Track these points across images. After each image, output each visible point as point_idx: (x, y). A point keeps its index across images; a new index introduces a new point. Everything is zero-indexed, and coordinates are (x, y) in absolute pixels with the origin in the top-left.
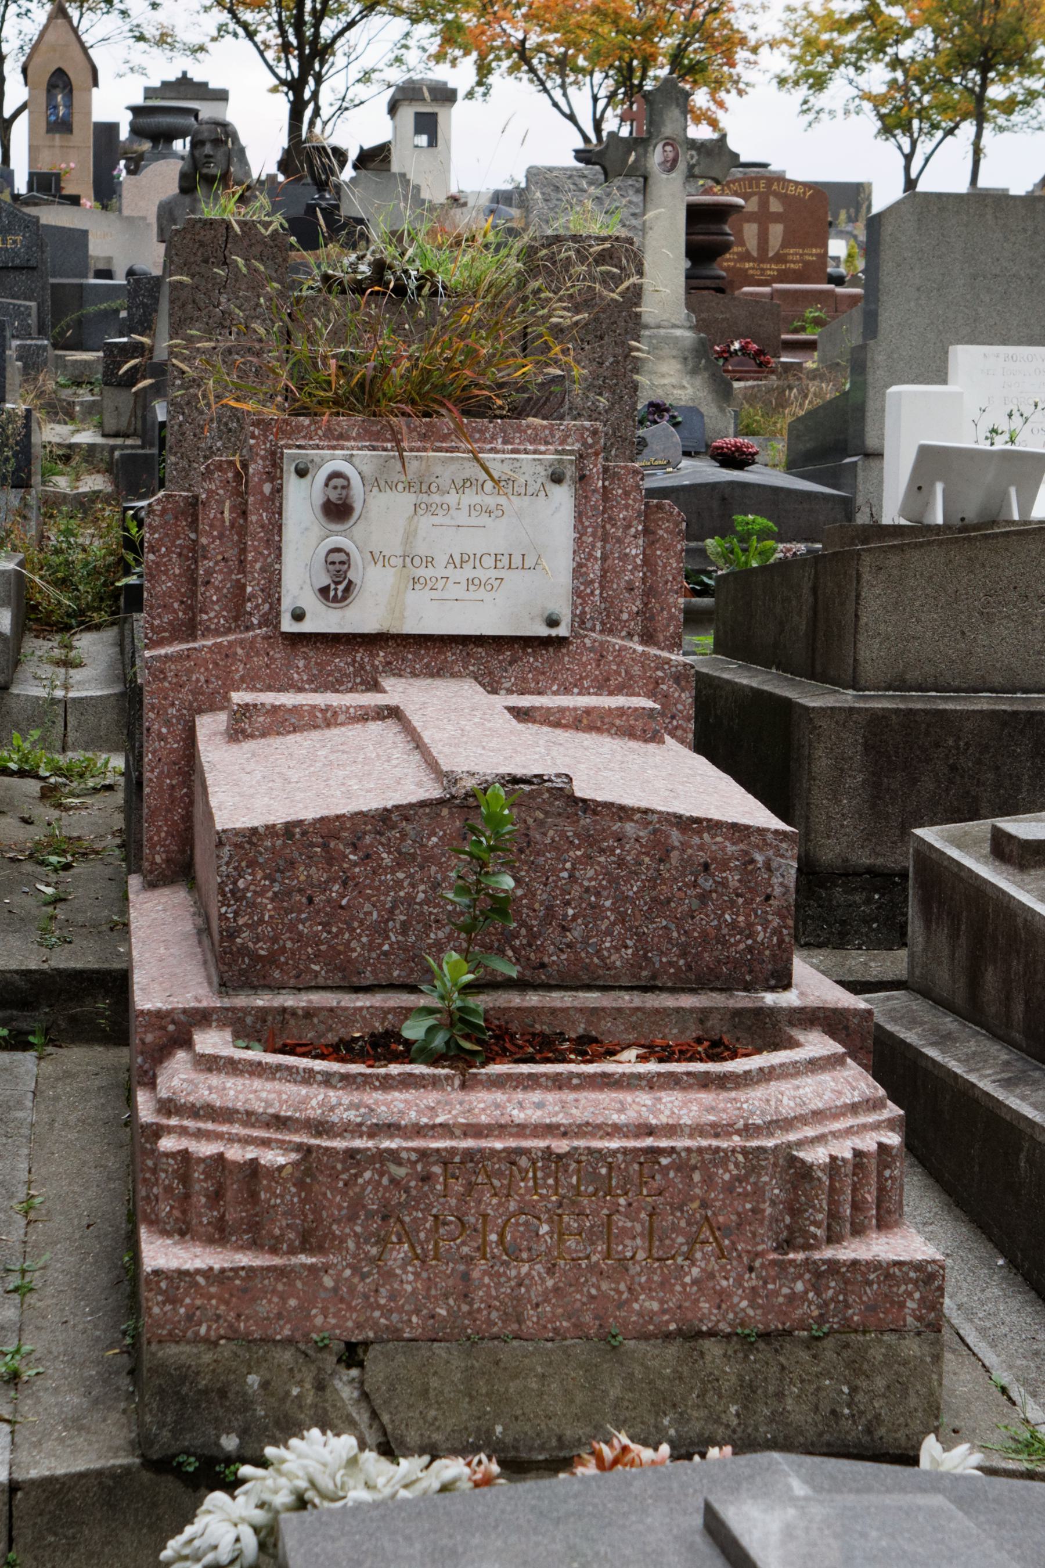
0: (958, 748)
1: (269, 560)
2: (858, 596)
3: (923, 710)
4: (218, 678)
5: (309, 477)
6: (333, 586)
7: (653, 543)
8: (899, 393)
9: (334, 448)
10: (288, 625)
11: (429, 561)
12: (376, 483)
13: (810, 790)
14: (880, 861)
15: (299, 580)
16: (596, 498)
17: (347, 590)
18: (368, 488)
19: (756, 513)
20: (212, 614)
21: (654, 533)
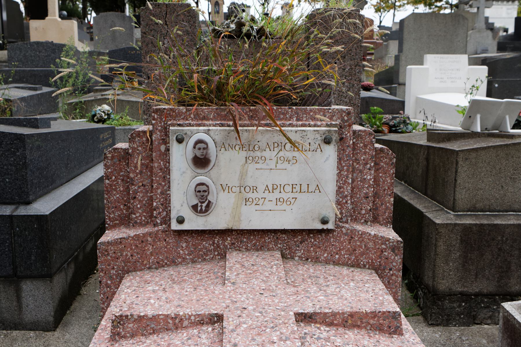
0: (503, 241)
1: (165, 188)
2: (456, 172)
3: (488, 224)
4: (138, 253)
5: (184, 143)
6: (199, 204)
7: (378, 170)
8: (411, 68)
9: (199, 125)
10: (175, 226)
11: (255, 189)
12: (223, 146)
13: (435, 260)
14: (466, 289)
15: (180, 202)
16: (349, 150)
17: (208, 206)
18: (219, 148)
19: (376, 106)
20: (138, 215)
21: (378, 164)
